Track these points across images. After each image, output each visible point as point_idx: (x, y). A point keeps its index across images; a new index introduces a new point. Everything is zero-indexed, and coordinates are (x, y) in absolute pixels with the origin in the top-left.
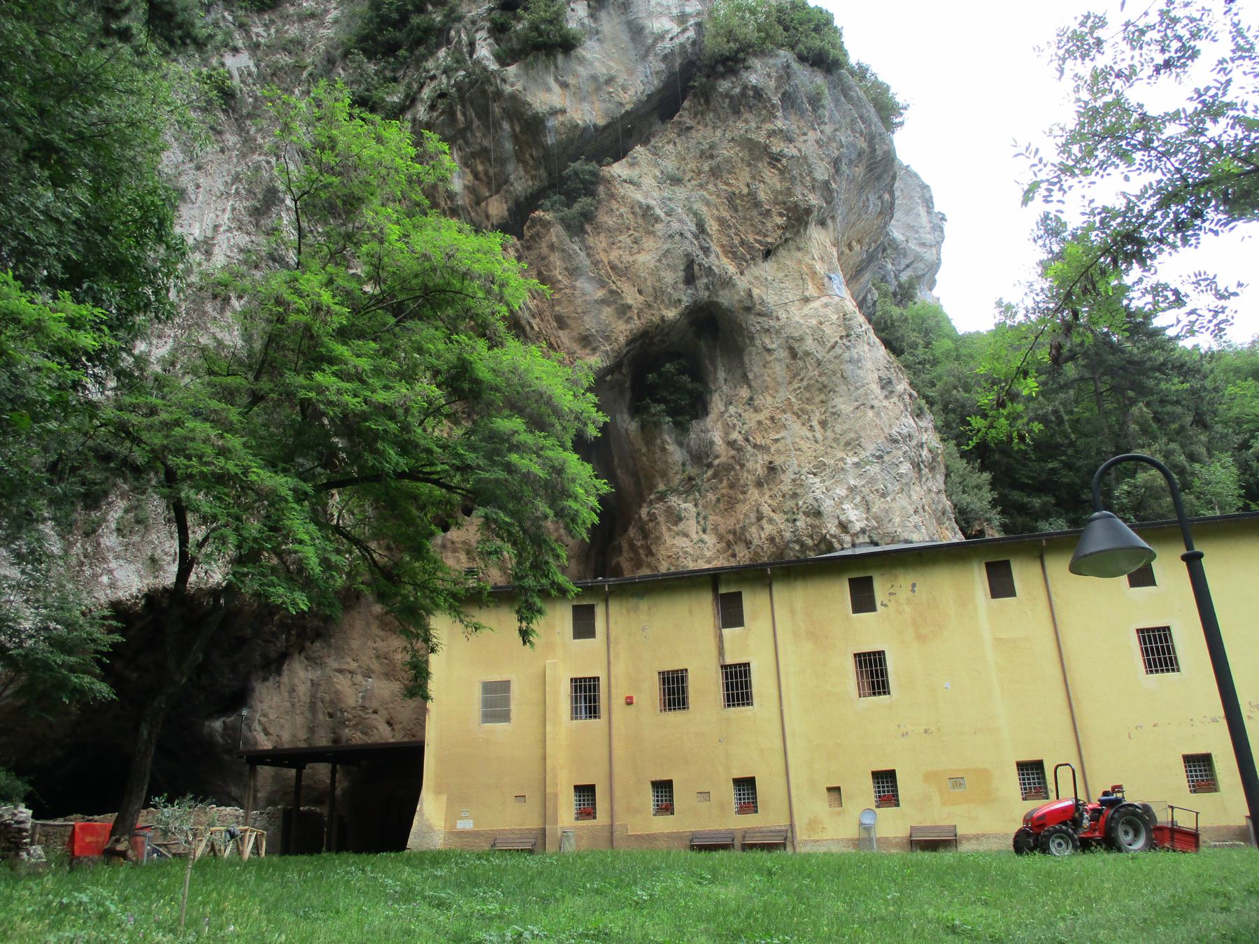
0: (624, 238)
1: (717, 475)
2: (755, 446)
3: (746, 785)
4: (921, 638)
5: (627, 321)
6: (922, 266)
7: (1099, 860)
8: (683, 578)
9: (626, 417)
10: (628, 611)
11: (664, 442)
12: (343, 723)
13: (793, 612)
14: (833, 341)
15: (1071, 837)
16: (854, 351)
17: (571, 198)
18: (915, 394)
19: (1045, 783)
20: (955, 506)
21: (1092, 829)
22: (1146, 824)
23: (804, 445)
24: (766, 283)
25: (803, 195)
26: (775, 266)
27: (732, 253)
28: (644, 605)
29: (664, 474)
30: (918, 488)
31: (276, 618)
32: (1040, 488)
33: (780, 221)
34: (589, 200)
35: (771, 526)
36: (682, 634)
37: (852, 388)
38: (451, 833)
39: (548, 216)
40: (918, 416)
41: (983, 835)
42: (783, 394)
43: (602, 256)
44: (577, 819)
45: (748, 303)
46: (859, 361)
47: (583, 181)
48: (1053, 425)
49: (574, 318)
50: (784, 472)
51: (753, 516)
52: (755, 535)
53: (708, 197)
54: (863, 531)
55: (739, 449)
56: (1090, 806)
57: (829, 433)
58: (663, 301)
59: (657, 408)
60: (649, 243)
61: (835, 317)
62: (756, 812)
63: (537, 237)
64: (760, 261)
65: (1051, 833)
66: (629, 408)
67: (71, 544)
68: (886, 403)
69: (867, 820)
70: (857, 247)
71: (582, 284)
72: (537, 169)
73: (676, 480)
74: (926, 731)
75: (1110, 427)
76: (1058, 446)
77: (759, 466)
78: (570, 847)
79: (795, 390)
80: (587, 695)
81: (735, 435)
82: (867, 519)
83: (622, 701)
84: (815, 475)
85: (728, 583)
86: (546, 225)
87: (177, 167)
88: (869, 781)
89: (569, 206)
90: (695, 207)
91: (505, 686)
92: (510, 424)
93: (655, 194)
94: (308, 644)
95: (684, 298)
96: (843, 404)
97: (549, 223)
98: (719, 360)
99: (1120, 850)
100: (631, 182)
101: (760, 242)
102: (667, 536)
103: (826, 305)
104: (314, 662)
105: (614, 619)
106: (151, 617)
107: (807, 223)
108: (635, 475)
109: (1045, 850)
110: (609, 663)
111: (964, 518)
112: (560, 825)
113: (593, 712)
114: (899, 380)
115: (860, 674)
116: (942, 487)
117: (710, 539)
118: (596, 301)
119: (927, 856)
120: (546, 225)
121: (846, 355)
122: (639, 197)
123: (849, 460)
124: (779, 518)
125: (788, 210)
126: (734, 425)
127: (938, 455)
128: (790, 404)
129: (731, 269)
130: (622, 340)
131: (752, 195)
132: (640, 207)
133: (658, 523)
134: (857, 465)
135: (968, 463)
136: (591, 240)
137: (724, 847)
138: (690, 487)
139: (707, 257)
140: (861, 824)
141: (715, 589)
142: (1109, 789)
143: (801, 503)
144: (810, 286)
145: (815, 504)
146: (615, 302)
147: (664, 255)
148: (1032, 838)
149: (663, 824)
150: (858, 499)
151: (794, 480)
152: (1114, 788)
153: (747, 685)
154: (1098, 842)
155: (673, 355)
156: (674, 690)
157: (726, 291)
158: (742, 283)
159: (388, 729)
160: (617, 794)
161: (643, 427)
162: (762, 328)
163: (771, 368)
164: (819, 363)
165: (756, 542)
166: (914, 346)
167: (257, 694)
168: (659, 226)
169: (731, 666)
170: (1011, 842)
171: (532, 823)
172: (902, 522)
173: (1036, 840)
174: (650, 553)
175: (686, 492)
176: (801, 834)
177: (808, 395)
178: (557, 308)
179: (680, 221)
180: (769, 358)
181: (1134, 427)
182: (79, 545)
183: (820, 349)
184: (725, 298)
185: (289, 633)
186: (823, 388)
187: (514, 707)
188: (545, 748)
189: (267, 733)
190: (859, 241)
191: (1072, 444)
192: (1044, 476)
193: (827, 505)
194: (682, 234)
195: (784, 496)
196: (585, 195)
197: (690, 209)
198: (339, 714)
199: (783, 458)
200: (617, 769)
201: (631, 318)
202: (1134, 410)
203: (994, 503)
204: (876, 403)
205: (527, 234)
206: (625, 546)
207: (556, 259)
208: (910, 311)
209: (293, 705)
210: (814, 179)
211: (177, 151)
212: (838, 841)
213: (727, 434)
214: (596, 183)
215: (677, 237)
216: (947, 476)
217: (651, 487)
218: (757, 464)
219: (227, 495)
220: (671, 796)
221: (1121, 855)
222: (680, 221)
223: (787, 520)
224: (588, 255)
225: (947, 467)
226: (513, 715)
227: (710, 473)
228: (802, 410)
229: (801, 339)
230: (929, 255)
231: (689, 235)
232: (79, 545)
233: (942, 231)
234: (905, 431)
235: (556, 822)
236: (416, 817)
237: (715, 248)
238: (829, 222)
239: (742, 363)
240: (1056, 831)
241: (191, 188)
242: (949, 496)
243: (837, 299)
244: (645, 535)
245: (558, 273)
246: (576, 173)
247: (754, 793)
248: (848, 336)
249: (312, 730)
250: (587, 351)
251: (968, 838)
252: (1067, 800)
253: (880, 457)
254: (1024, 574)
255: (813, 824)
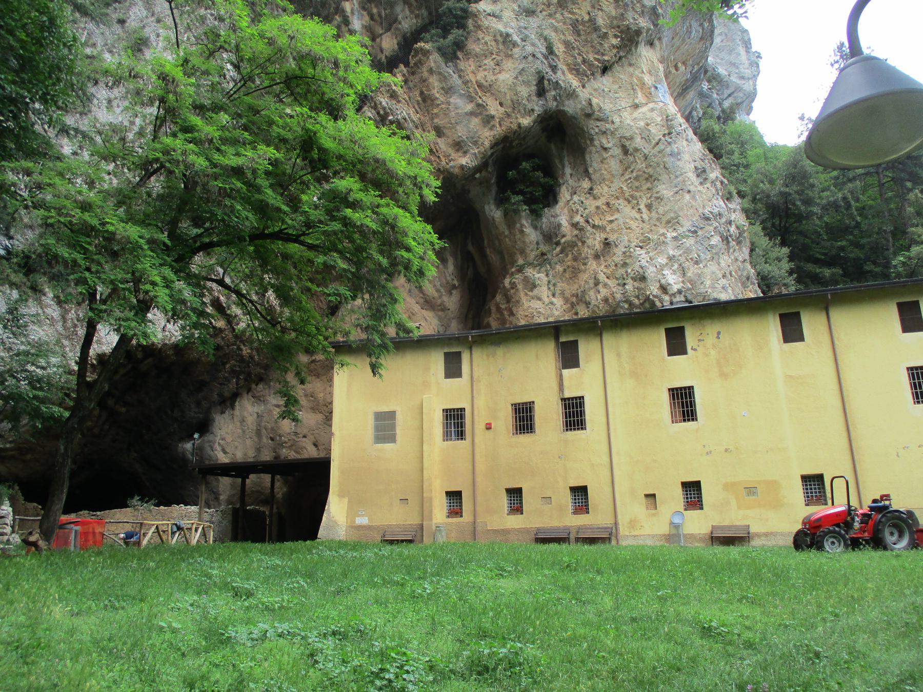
0: (489, 62)
1: (561, 248)
2: (594, 226)
3: (580, 492)
4: (723, 375)
5: (491, 129)
6: (741, 95)
7: (867, 557)
8: (531, 330)
9: (493, 207)
10: (488, 356)
11: (522, 226)
12: (281, 445)
13: (619, 355)
14: (657, 138)
15: (843, 537)
16: (674, 147)
17: (446, 32)
18: (725, 181)
19: (825, 492)
20: (758, 274)
21: (862, 530)
22: (909, 527)
23: (633, 224)
24: (602, 93)
25: (634, 19)
26: (611, 80)
27: (575, 70)
28: (500, 351)
29: (523, 252)
30: (726, 258)
31: (227, 366)
32: (830, 262)
33: (615, 41)
34: (461, 32)
35: (605, 288)
36: (532, 374)
37: (673, 177)
38: (352, 527)
39: (427, 46)
40: (727, 199)
41: (772, 533)
42: (618, 184)
43: (471, 77)
44: (448, 517)
45: (589, 111)
46: (679, 154)
47: (456, 16)
48: (843, 210)
49: (450, 128)
50: (616, 246)
51: (591, 282)
52: (593, 297)
53: (556, 24)
54: (680, 292)
55: (581, 229)
56: (861, 511)
57: (654, 214)
58: (519, 111)
59: (515, 199)
60: (508, 64)
61: (659, 119)
62: (588, 513)
63: (419, 64)
64: (598, 76)
65: (826, 534)
66: (495, 200)
67: (67, 311)
68: (700, 188)
69: (677, 520)
70: (682, 68)
71: (455, 100)
72: (419, 8)
73: (532, 256)
74: (726, 450)
75: (890, 210)
76: (847, 227)
77: (597, 243)
78: (441, 539)
79: (626, 180)
80: (455, 421)
81: (578, 218)
82: (683, 282)
83: (483, 426)
84: (641, 248)
85: (567, 333)
86: (426, 53)
87: (142, 21)
88: (679, 490)
89: (444, 38)
90: (546, 33)
91: (392, 415)
92: (347, 183)
93: (514, 24)
94: (253, 386)
95: (536, 108)
96: (665, 190)
97: (428, 51)
98: (566, 158)
99: (885, 548)
100: (494, 16)
101: (598, 60)
102: (524, 300)
103: (652, 110)
104: (259, 399)
105: (477, 362)
106: (130, 367)
107: (637, 43)
108: (500, 253)
109: (820, 548)
110: (472, 397)
111: (765, 281)
112: (434, 521)
113: (461, 435)
114: (712, 170)
115: (673, 405)
116: (747, 257)
117: (558, 302)
118: (466, 114)
119: (719, 550)
120: (426, 53)
121: (668, 150)
122: (500, 27)
123: (669, 235)
124: (611, 283)
125: (621, 32)
126: (578, 210)
127: (744, 231)
128: (623, 192)
129: (575, 83)
130: (487, 144)
131: (592, 21)
132: (501, 35)
133: (517, 290)
134: (675, 238)
135: (770, 239)
136: (462, 65)
137: (558, 540)
138: (542, 260)
139: (555, 73)
140: (671, 523)
141: (557, 338)
142: (878, 497)
143: (629, 271)
144: (640, 94)
145: (641, 271)
146: (481, 114)
147: (520, 73)
148: (809, 537)
149: (514, 522)
150: (676, 266)
151: (624, 253)
152: (882, 497)
153: (582, 413)
154: (867, 542)
155: (528, 157)
156: (524, 418)
157: (571, 102)
158: (583, 94)
159: (314, 449)
160: (479, 498)
161: (506, 214)
162: (600, 130)
163: (606, 163)
164: (646, 157)
165: (593, 303)
166: (731, 153)
167: (217, 423)
168: (516, 50)
169: (569, 399)
170: (791, 539)
171: (413, 520)
172: (713, 284)
173: (812, 539)
174: (512, 314)
175: (539, 265)
176: (623, 530)
177: (637, 184)
178: (436, 121)
179: (533, 45)
180: (605, 155)
181: (910, 210)
182: (73, 312)
183: (647, 145)
184: (570, 107)
185: (238, 378)
186: (649, 178)
187: (399, 431)
188: (422, 462)
189: (225, 452)
190: (684, 63)
191: (858, 225)
192: (834, 252)
193: (651, 272)
194: (534, 56)
195: (616, 265)
196: (458, 28)
197: (541, 35)
198: (278, 438)
199: (616, 236)
200: (479, 479)
201: (494, 126)
202: (911, 196)
203: (791, 273)
204: (692, 188)
205: (412, 62)
206: (493, 309)
207: (434, 81)
208: (730, 127)
209: (244, 432)
210: (643, 6)
211: (142, 9)
212: (653, 536)
213: (572, 217)
214: (466, 18)
215: (530, 58)
216: (752, 250)
217: (513, 262)
218: (595, 241)
219: (89, 244)
220: (521, 500)
221: (887, 553)
222: (533, 45)
223: (619, 285)
224: (460, 76)
225: (752, 244)
226: (398, 437)
227: (558, 249)
228: (632, 196)
229: (631, 138)
230: (747, 86)
231: (540, 56)
232: (73, 312)
233: (758, 66)
234: (716, 210)
235: (431, 519)
236: (325, 515)
237: (561, 66)
238: (656, 42)
239: (585, 160)
240: (830, 532)
241: (153, 37)
242: (754, 266)
243: (661, 104)
244: (508, 299)
245: (436, 93)
246: (450, 10)
247: (587, 498)
248: (669, 134)
249: (258, 450)
250: (460, 154)
251: (758, 535)
252: (840, 506)
253: (695, 232)
254: (812, 323)
255: (632, 523)
